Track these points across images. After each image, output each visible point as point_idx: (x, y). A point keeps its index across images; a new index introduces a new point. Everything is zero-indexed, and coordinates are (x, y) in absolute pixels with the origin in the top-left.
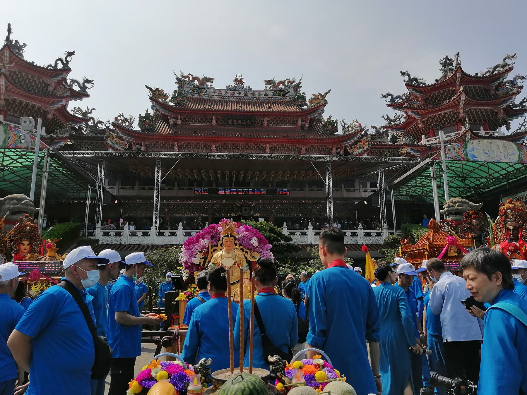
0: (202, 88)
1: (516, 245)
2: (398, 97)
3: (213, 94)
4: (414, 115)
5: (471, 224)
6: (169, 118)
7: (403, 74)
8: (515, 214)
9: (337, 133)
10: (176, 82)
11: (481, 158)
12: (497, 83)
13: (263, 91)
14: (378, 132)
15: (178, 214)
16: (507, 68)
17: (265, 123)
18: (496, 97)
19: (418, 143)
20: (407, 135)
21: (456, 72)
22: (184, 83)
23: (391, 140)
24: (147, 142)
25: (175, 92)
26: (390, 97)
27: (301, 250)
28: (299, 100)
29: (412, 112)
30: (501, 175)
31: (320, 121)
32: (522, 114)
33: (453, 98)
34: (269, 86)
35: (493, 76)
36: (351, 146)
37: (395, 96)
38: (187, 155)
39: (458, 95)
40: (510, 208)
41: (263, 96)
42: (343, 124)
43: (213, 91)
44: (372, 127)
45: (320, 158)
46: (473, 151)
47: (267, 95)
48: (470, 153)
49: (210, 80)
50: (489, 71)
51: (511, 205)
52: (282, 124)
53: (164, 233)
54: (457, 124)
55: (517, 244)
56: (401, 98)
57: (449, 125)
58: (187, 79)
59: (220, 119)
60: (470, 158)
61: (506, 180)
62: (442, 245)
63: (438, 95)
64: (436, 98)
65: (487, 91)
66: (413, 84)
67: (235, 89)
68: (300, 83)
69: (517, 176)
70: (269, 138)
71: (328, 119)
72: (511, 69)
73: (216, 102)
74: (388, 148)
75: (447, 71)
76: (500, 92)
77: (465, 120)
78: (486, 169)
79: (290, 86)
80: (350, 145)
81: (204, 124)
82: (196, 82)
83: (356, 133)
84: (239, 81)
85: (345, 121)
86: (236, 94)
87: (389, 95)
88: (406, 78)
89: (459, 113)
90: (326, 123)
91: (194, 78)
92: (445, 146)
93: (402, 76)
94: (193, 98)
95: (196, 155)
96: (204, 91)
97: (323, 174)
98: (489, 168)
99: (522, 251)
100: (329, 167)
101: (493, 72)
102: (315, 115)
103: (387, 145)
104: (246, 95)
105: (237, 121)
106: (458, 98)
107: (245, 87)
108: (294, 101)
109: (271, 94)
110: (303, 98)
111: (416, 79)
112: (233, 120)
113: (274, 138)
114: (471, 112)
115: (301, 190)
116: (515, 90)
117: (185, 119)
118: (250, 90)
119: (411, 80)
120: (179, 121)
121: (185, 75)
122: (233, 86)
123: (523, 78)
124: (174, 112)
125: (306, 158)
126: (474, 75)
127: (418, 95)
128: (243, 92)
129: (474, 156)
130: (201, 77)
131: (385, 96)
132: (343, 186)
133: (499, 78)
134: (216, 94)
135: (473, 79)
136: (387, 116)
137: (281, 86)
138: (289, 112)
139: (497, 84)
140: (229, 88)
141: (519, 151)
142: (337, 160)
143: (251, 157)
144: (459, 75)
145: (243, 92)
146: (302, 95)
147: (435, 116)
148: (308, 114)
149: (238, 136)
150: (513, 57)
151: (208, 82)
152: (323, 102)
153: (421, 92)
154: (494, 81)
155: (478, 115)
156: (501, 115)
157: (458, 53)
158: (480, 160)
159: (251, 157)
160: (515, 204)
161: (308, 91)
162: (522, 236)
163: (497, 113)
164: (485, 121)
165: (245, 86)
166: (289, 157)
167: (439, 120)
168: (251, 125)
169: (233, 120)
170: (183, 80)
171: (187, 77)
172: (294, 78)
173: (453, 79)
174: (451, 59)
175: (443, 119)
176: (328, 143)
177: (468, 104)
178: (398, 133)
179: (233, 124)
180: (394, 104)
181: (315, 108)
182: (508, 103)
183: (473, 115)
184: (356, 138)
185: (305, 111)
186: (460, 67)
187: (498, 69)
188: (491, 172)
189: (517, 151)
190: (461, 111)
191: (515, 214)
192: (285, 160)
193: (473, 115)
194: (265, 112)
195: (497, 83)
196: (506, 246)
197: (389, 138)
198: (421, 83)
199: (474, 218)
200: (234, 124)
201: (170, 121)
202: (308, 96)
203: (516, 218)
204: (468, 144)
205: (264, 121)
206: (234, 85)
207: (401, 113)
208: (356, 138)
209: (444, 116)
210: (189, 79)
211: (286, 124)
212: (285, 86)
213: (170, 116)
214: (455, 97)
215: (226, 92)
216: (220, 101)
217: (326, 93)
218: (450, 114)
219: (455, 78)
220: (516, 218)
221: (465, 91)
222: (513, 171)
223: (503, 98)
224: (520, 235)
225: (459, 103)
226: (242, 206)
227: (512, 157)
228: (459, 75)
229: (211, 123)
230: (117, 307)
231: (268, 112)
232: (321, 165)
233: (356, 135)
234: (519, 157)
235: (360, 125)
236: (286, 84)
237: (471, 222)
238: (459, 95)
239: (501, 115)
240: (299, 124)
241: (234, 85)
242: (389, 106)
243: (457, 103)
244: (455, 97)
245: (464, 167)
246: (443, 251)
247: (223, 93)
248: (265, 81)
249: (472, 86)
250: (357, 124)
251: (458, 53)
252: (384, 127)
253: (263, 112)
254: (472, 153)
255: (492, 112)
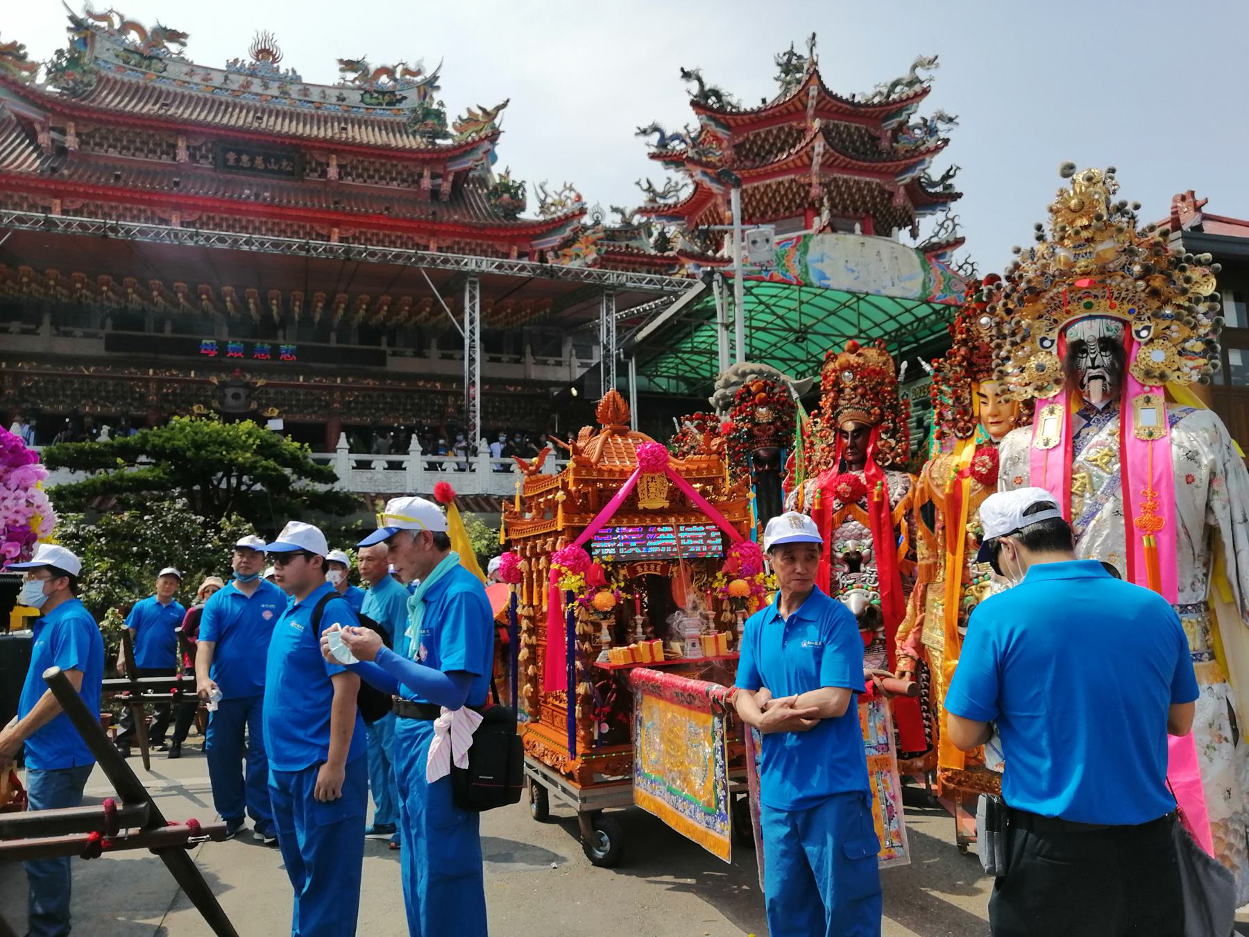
0: (151, 58)
1: (857, 479)
2: (676, 137)
3: (187, 79)
4: (707, 183)
5: (752, 420)
6: (38, 127)
7: (686, 75)
8: (863, 385)
9: (522, 216)
10: (69, 29)
11: (841, 280)
12: (894, 123)
13: (334, 87)
14: (627, 223)
15: (51, 404)
16: (917, 88)
17: (333, 172)
18: (893, 155)
19: (716, 251)
20: (692, 232)
21: (807, 82)
22: (93, 35)
23: (656, 246)
24: (68, 204)
25: (60, 53)
26: (657, 136)
27: (362, 506)
28: (429, 121)
29: (705, 173)
30: (886, 333)
31: (483, 182)
32: (944, 203)
33: (798, 147)
34: (351, 76)
35: (888, 104)
36: (555, 250)
37: (669, 133)
38: (38, 221)
39: (808, 139)
40: (848, 367)
41: (334, 100)
42: (542, 196)
43: (186, 69)
44: (615, 210)
45: (446, 261)
46: (822, 261)
47: (344, 100)
48: (814, 267)
49: (176, 36)
50: (880, 93)
51: (853, 359)
52: (381, 178)
53: (402, 463)
54: (804, 214)
55: (862, 477)
56: (683, 141)
57: (787, 214)
58: (104, 24)
59: (199, 148)
60: (813, 278)
61: (895, 346)
62: (622, 472)
63: (766, 139)
64: (762, 146)
65: (875, 140)
66: (707, 102)
67: (253, 72)
68: (435, 77)
69: (919, 335)
70: (336, 210)
71: (501, 176)
72: (925, 92)
73: (191, 101)
74: (648, 264)
75: (789, 83)
76: (903, 145)
77: (822, 204)
78: (852, 316)
79: (408, 83)
80: (553, 249)
81: (153, 159)
82: (133, 36)
83: (568, 219)
84: (265, 53)
85: (546, 188)
86: (256, 87)
87: (656, 129)
88: (694, 87)
89: (810, 185)
90: (495, 188)
91: (128, 26)
92: (743, 231)
93: (684, 81)
94: (123, 84)
95: (69, 225)
96: (157, 65)
97: (458, 311)
98: (860, 314)
99: (871, 499)
100: (475, 289)
101: (888, 96)
102: (467, 163)
103: (644, 255)
104: (285, 93)
105: (252, 160)
106: (808, 148)
107: (282, 71)
108: (416, 121)
109: (354, 98)
110: (439, 115)
111: (716, 93)
112: (239, 153)
113: (351, 214)
114: (837, 187)
115: (419, 354)
116: (931, 143)
117: (90, 135)
118: (296, 79)
119: (704, 94)
120: (71, 142)
121: (99, 9)
122: (247, 64)
123: (951, 120)
124: (52, 111)
125: (409, 258)
126: (846, 95)
127: (721, 132)
128: (277, 84)
129: (823, 276)
130: (149, 25)
131: (644, 132)
132: (528, 350)
133: (899, 112)
134: (197, 79)
135: (845, 106)
136: (648, 182)
137: (384, 79)
138: (397, 149)
139: (895, 125)
140: (234, 67)
141: (925, 270)
142: (492, 269)
143: (246, 243)
144: (813, 91)
145: (277, 84)
146: (435, 106)
147: (757, 188)
148: (453, 158)
149: (248, 197)
150: (931, 62)
151: (171, 40)
152: (487, 131)
153: (727, 127)
154: (889, 117)
155: (851, 195)
156: (900, 200)
157: (814, 35)
158: (835, 286)
159: (246, 243)
160: (866, 357)
161: (455, 102)
162: (876, 452)
163: (891, 194)
164: (867, 211)
165: (284, 66)
166: (360, 253)
167: (766, 201)
168: (291, 173)
169: (239, 153)
170: (92, 26)
171: (104, 17)
172: (419, 63)
173: (800, 100)
174: (800, 57)
175: (774, 197)
176: (496, 238)
177: (830, 166)
178: (672, 229)
179: (238, 167)
180: (664, 155)
181: (467, 144)
182: (917, 172)
183: (840, 194)
184: (568, 232)
185: (448, 149)
186: (816, 72)
187: (898, 89)
188: (865, 324)
189: (920, 270)
190: (815, 180)
191: (863, 385)
192: (349, 259)
193: (840, 194)
194: (331, 141)
195: (894, 123)
196: (830, 483)
197: (652, 240)
198: (729, 104)
199: (763, 403)
200: (243, 168)
201: (43, 138)
202: (453, 114)
203: (863, 396)
204: (811, 244)
205: (328, 165)
206: (249, 60)
207: (678, 176)
208: (568, 232)
209: (777, 190)
210: (111, 25)
211: (392, 179)
212: (395, 80)
213: (40, 123)
214: (803, 143)
215: (226, 78)
216: (206, 100)
217: (498, 109)
218: (790, 188)
219: (804, 99)
220: (863, 396)
221: (825, 131)
222: (912, 323)
223: (906, 158)
224: (870, 450)
225: (811, 160)
226: (223, 385)
227: (908, 284)
228: (813, 91)
229: (174, 159)
230: (116, 659)
231: (339, 142)
232: (453, 284)
233: (566, 224)
234: (924, 286)
235: (579, 198)
236: (398, 76)
237: (753, 414)
238: (812, 140)
239: (900, 200)
240: (426, 183)
241: (249, 60)
242: (653, 156)
243: (805, 159)
244: (803, 143)
245: (805, 308)
246: (621, 492)
247: (218, 80)
248: (341, 61)
249: (843, 123)
250: (573, 195)
251: (814, 35)
252: (641, 211)
253: (324, 140)
254: (819, 266)
255: (882, 192)
